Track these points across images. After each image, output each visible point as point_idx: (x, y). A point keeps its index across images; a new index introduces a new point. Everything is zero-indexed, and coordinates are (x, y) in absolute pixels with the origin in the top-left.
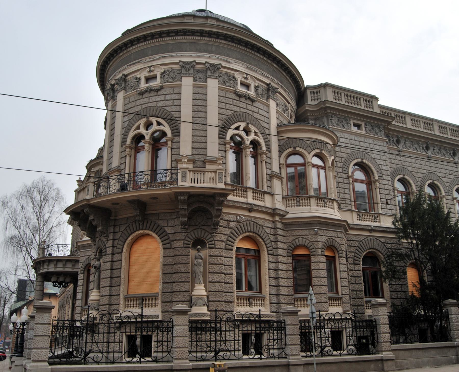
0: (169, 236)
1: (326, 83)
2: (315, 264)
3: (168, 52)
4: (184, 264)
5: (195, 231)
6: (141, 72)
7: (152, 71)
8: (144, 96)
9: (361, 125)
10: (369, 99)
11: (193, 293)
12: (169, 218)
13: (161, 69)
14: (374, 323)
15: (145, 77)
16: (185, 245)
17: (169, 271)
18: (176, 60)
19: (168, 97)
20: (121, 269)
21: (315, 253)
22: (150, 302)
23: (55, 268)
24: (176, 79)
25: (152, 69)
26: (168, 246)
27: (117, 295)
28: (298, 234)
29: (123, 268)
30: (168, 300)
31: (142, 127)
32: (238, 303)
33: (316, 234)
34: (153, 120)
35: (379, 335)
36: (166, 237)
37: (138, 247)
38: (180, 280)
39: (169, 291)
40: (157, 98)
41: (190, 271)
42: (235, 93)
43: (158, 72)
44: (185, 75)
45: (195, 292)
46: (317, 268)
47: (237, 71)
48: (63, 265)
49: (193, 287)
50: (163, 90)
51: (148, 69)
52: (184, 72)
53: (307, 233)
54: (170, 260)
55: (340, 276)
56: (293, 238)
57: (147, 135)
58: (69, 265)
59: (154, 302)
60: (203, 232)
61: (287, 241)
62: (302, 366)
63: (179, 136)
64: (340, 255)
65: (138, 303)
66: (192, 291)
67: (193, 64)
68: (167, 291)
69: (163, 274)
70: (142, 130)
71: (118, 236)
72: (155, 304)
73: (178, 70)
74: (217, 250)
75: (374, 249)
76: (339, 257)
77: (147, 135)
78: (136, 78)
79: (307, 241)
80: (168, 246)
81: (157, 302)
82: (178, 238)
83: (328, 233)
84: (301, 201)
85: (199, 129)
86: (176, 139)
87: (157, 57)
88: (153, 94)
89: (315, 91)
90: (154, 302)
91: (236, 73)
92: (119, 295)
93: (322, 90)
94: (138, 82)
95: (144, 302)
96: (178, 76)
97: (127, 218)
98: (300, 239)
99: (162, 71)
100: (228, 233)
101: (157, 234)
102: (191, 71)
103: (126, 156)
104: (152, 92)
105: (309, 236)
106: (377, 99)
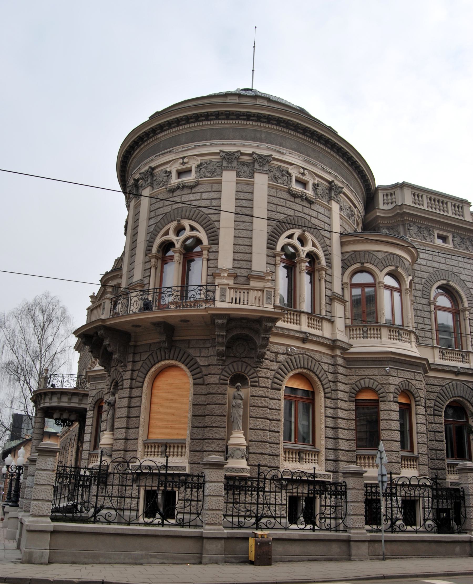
0: (201, 369)
1: (403, 182)
2: (385, 412)
3: (206, 140)
4: (220, 404)
5: (235, 364)
6: (172, 164)
7: (185, 163)
8: (175, 194)
9: (448, 237)
10: (459, 204)
11: (230, 442)
12: (202, 346)
13: (198, 161)
14: (461, 493)
15: (177, 171)
16: (222, 381)
17: (200, 413)
18: (216, 149)
19: (205, 196)
20: (140, 407)
21: (385, 399)
22: (176, 450)
23: (59, 402)
24: (215, 174)
25: (186, 160)
26: (200, 381)
27: (134, 439)
28: (364, 373)
29: (143, 406)
30: (198, 449)
31: (171, 232)
32: (285, 458)
33: (388, 374)
34: (186, 223)
35: (467, 509)
36: (198, 370)
37: (162, 382)
38: (214, 425)
39: (200, 437)
40: (192, 197)
41: (226, 414)
42: (289, 193)
43: (193, 164)
44: (227, 169)
45: (232, 441)
46: (387, 418)
47: (292, 164)
48: (80, 400)
49: (229, 434)
50: (199, 187)
51: (181, 161)
52: (225, 164)
53: (376, 373)
54: (202, 399)
55: (417, 430)
56: (358, 378)
57: (178, 242)
58: (75, 400)
59: (180, 450)
60: (245, 365)
61: (350, 382)
62: (367, 544)
63: (218, 244)
64: (418, 403)
65: (160, 450)
66: (228, 439)
67: (237, 154)
68: (197, 437)
69: (193, 416)
70: (172, 237)
71: (138, 366)
72: (181, 453)
73: (218, 162)
74: (261, 389)
75: (461, 397)
76: (416, 405)
77: (178, 242)
78: (166, 172)
79: (376, 383)
80: (200, 381)
81: (184, 451)
82: (213, 372)
83: (402, 374)
84: (369, 332)
85: (243, 236)
86: (214, 248)
87: (192, 145)
88: (186, 191)
89: (389, 192)
90: (180, 450)
91: (291, 167)
92: (137, 439)
93: (398, 192)
94: (168, 176)
95: (168, 450)
96: (218, 170)
97: (150, 345)
98: (367, 380)
99: (199, 163)
100: (275, 369)
101: (186, 366)
102: (235, 164)
103: (150, 268)
104: (185, 189)
105: (378, 377)
106: (469, 204)
